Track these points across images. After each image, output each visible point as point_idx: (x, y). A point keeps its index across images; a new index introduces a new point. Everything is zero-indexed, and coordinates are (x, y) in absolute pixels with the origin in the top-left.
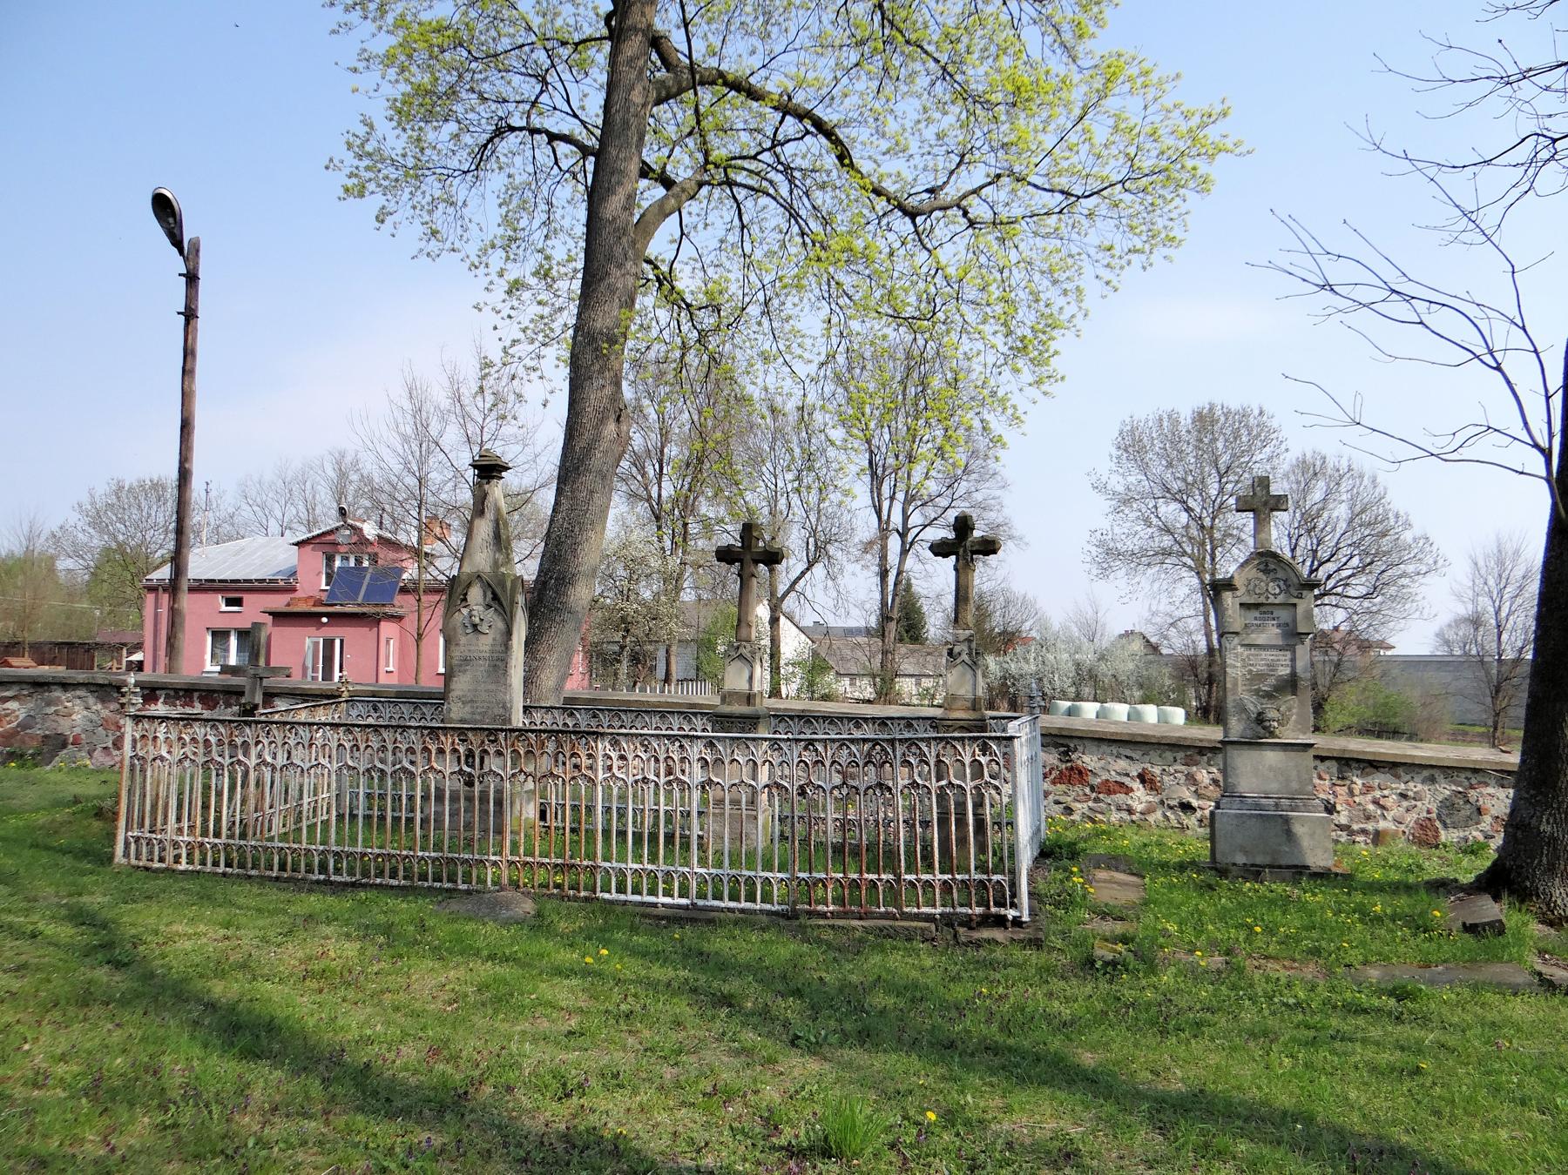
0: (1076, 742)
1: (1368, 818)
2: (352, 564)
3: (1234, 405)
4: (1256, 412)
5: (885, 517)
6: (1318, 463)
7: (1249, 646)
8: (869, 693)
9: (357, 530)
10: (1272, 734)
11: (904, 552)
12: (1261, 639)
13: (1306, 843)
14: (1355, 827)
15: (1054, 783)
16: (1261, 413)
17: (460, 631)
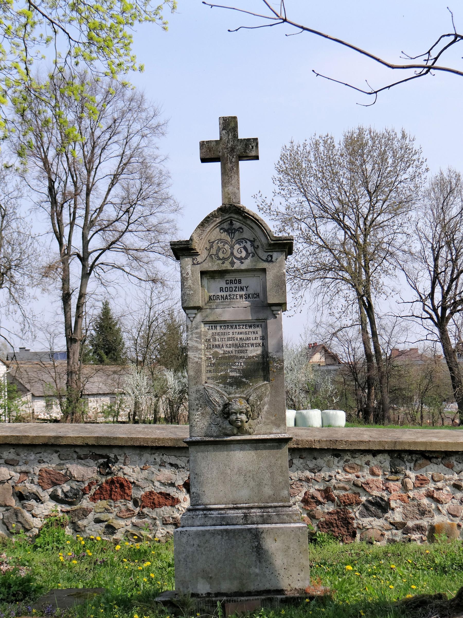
0: (115, 451)
1: (423, 513)
3: (379, 129)
4: (399, 136)
5: (65, 241)
6: (454, 181)
7: (214, 323)
8: (56, 412)
10: (241, 430)
11: (86, 275)
12: (227, 313)
13: (279, 561)
14: (410, 524)
15: (93, 499)
16: (404, 136)
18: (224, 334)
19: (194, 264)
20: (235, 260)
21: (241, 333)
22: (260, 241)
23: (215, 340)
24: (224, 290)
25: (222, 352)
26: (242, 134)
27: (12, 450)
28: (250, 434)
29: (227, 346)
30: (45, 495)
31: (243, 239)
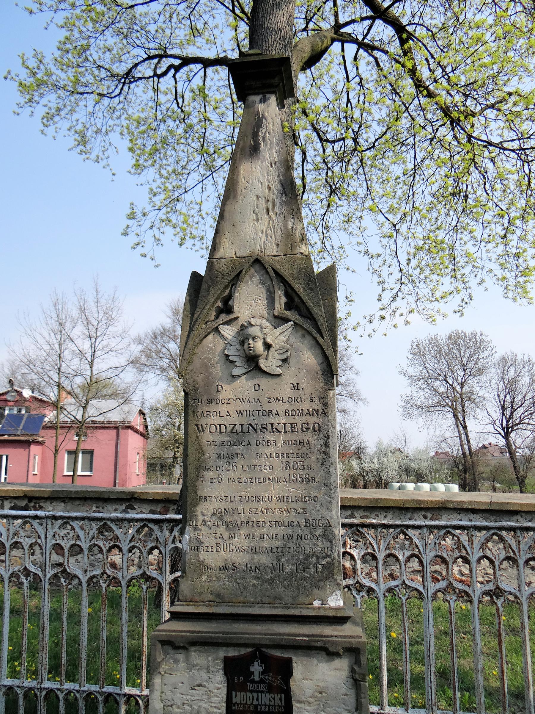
2: (15, 412)
4: (479, 334)
9: (20, 394)
16: (482, 334)
17: (219, 370)
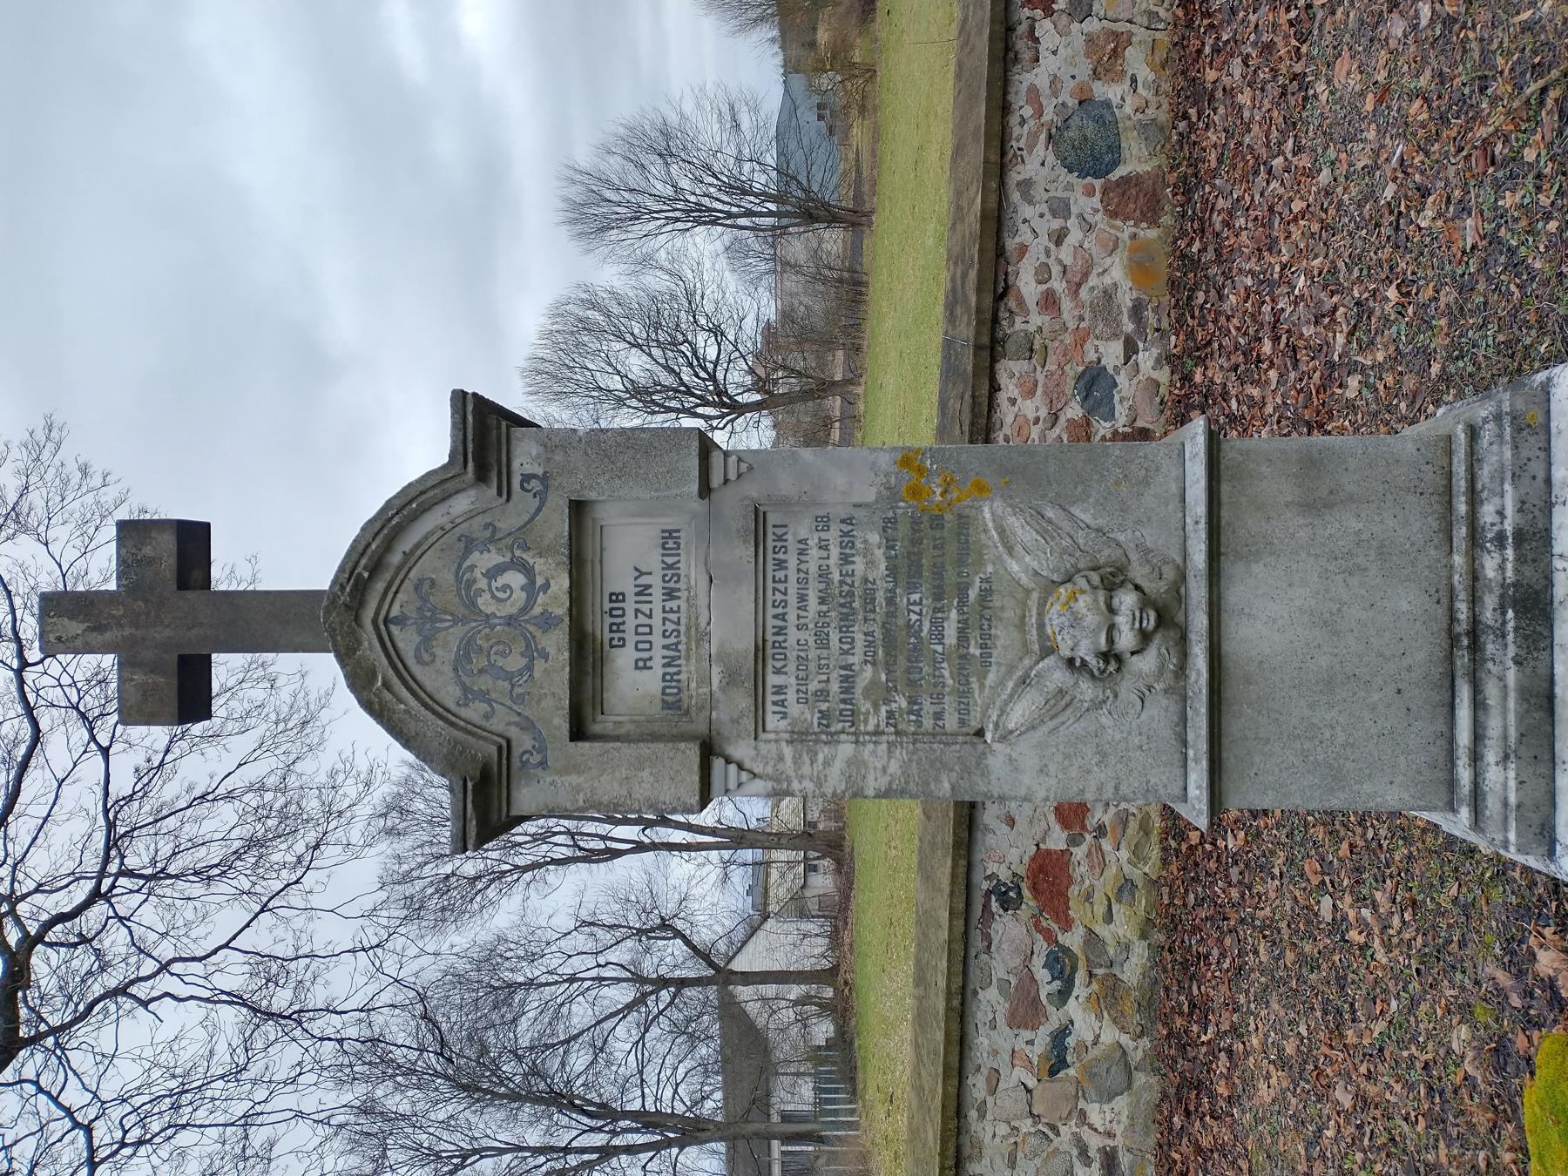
18: (802, 661)
19: (543, 764)
20: (537, 610)
21: (802, 598)
22: (470, 516)
23: (823, 694)
24: (645, 655)
25: (868, 672)
26: (100, 570)
27: (970, 1081)
28: (1183, 577)
29: (846, 652)
30: (1055, 1018)
31: (458, 579)
